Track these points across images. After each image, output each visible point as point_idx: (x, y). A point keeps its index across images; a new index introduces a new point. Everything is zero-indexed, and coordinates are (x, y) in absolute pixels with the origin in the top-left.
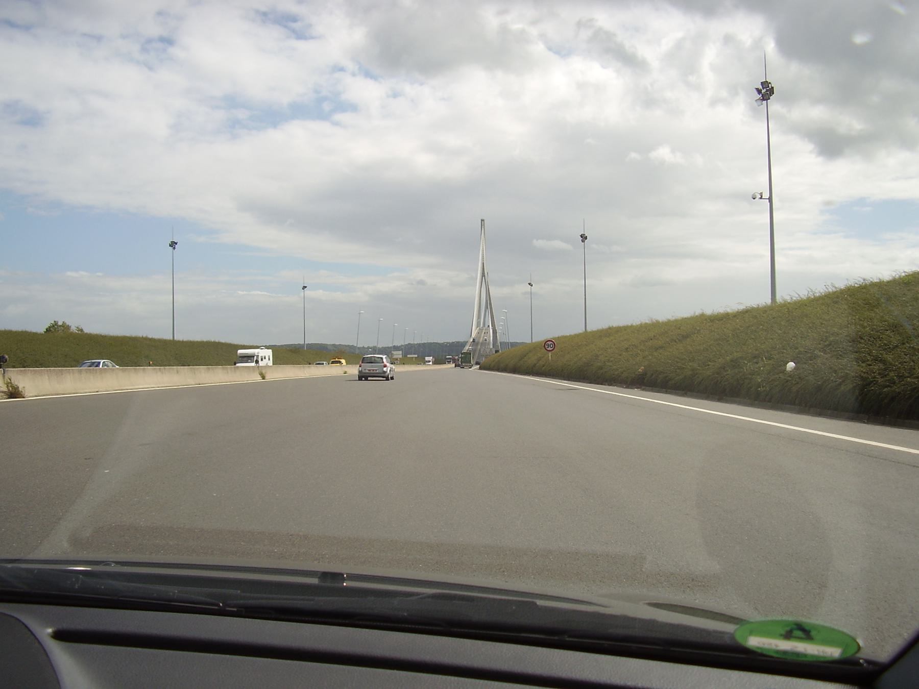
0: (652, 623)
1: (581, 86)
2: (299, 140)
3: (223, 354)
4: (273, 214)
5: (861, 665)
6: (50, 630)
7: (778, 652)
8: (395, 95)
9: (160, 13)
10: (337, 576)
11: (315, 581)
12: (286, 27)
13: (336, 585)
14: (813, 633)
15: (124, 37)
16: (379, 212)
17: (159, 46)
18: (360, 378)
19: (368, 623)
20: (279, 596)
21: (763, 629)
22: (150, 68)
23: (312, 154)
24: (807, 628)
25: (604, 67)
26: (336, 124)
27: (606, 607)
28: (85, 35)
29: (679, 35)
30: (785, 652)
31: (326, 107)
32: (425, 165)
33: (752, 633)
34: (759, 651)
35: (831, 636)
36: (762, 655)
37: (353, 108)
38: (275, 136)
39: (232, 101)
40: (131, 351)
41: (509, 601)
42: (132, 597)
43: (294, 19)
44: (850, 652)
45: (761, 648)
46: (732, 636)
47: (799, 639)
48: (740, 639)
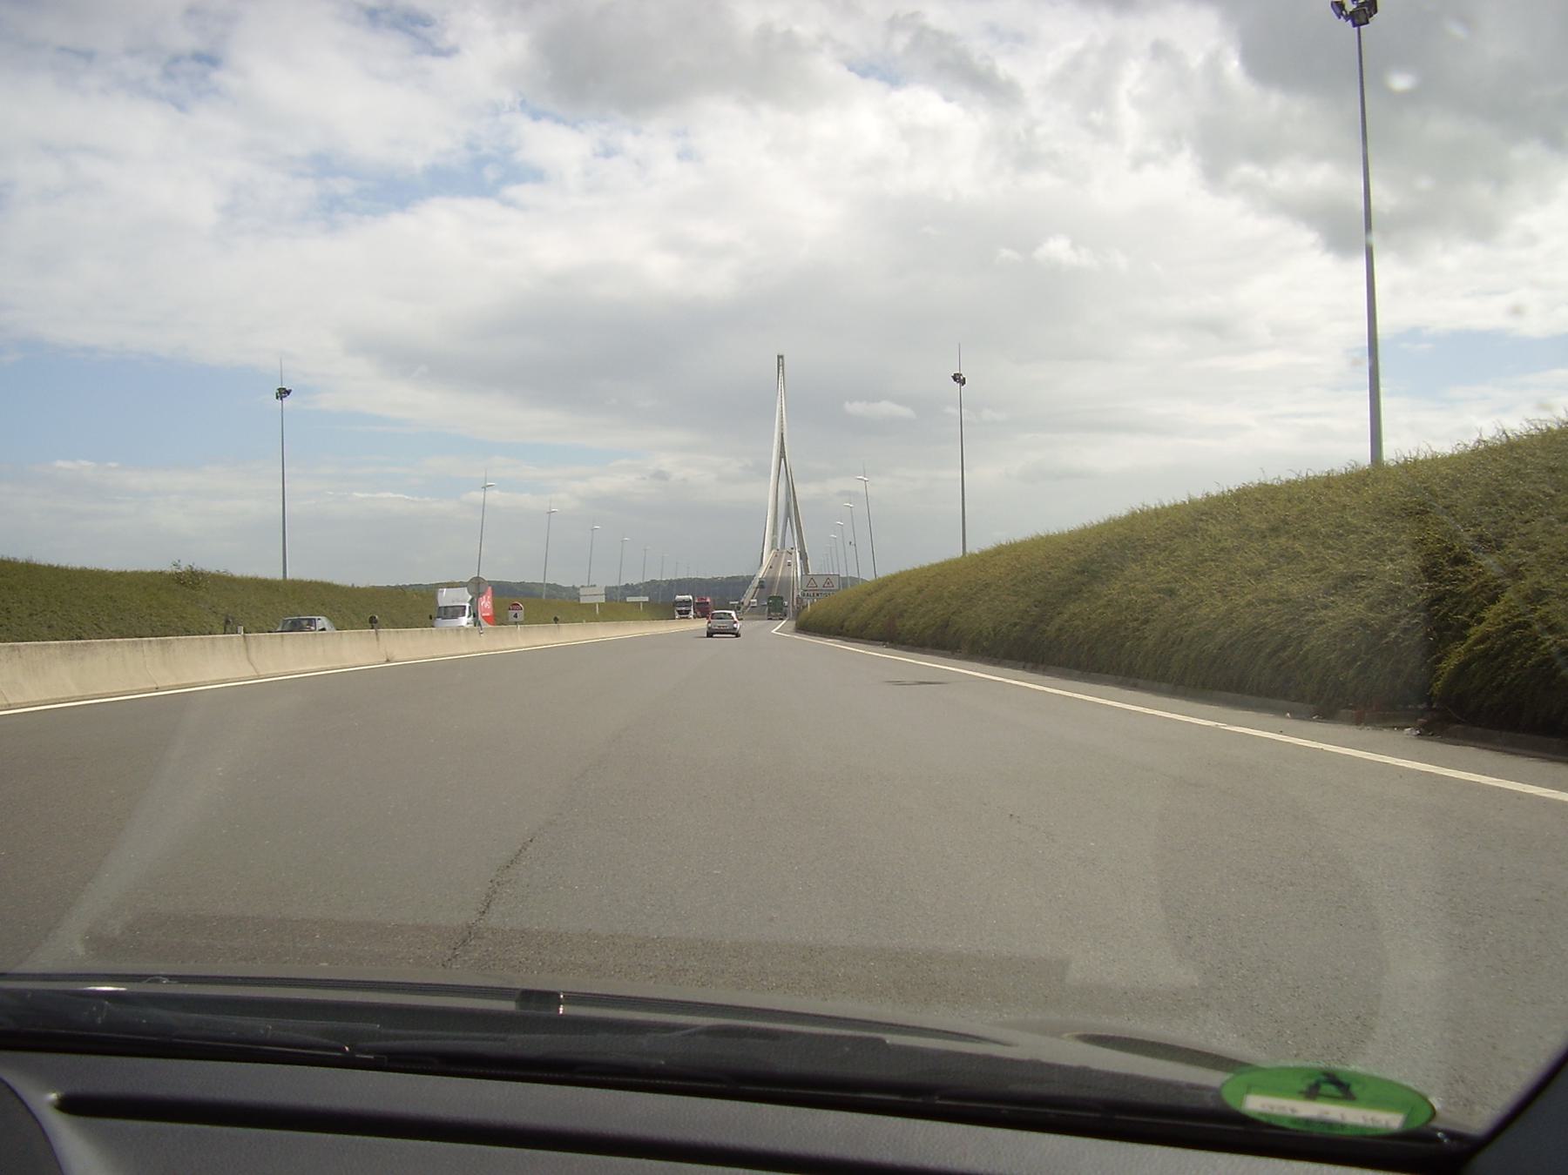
0: (1083, 1073)
1: (910, 133)
2: (443, 230)
3: (410, 607)
4: (403, 359)
5: (1438, 1140)
6: (53, 1096)
7: (1297, 1120)
8: (608, 153)
9: (191, 11)
10: (550, 998)
11: (509, 1006)
12: (413, 34)
13: (544, 1013)
14: (1355, 1089)
15: (132, 52)
16: (585, 355)
17: (192, 68)
19: (523, 1073)
20: (445, 1034)
21: (1274, 1082)
22: (181, 108)
23: (470, 259)
24: (1344, 1080)
25: (948, 99)
26: (509, 203)
27: (1009, 1045)
28: (63, 49)
29: (1077, 44)
30: (1308, 1121)
31: (490, 174)
32: (662, 272)
33: (1250, 1089)
34: (1263, 1119)
36: (1270, 1126)
37: (536, 175)
38: (402, 225)
39: (324, 165)
41: (838, 1037)
43: (426, 21)
44: (1418, 1121)
46: (1216, 1093)
47: (1331, 1098)
48: (1231, 1099)
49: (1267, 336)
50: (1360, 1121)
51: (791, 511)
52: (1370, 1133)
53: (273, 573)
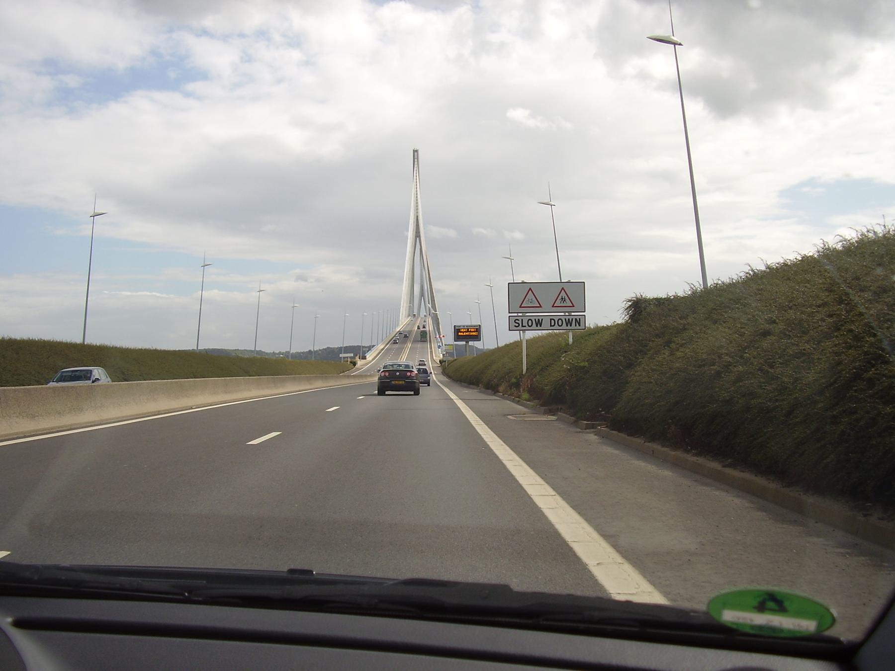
2: (142, 111)
6: (10, 620)
7: (754, 627)
14: (786, 604)
16: (257, 198)
18: (383, 388)
24: (779, 598)
26: (188, 95)
30: (761, 627)
31: (172, 74)
34: (735, 627)
35: (806, 609)
37: (203, 75)
38: (117, 110)
39: (53, 65)
40: (138, 366)
42: (97, 588)
45: (736, 624)
47: (772, 611)
48: (714, 614)
49: (722, 191)
50: (791, 627)
51: (424, 294)
52: (798, 635)
53: (75, 338)
